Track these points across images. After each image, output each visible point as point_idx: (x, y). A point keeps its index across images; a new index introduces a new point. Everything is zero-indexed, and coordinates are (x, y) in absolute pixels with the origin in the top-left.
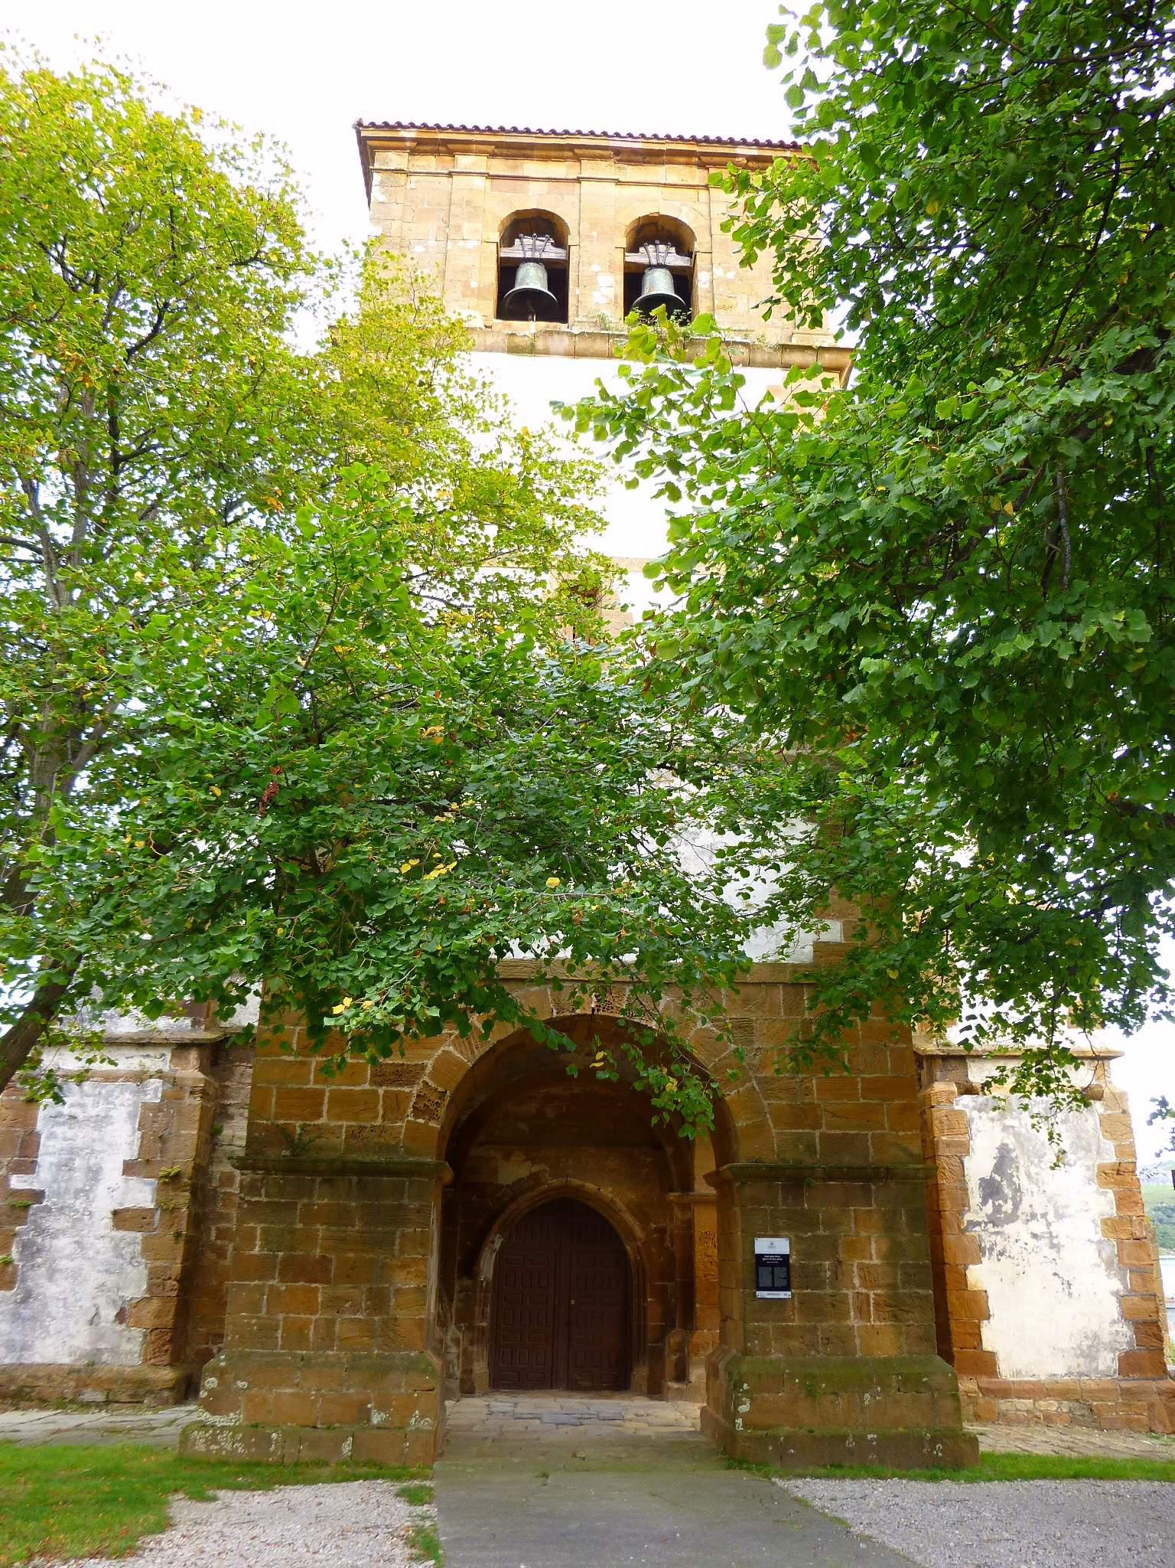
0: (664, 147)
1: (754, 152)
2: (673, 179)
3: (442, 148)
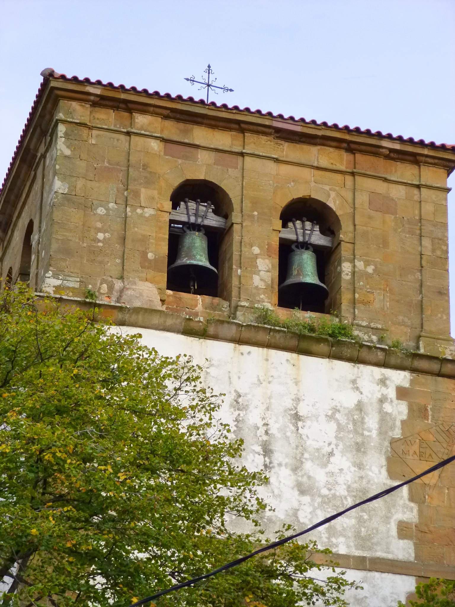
0: (320, 133)
1: (397, 146)
2: (324, 162)
3: (122, 105)
